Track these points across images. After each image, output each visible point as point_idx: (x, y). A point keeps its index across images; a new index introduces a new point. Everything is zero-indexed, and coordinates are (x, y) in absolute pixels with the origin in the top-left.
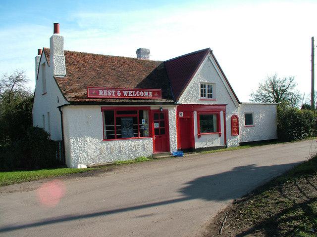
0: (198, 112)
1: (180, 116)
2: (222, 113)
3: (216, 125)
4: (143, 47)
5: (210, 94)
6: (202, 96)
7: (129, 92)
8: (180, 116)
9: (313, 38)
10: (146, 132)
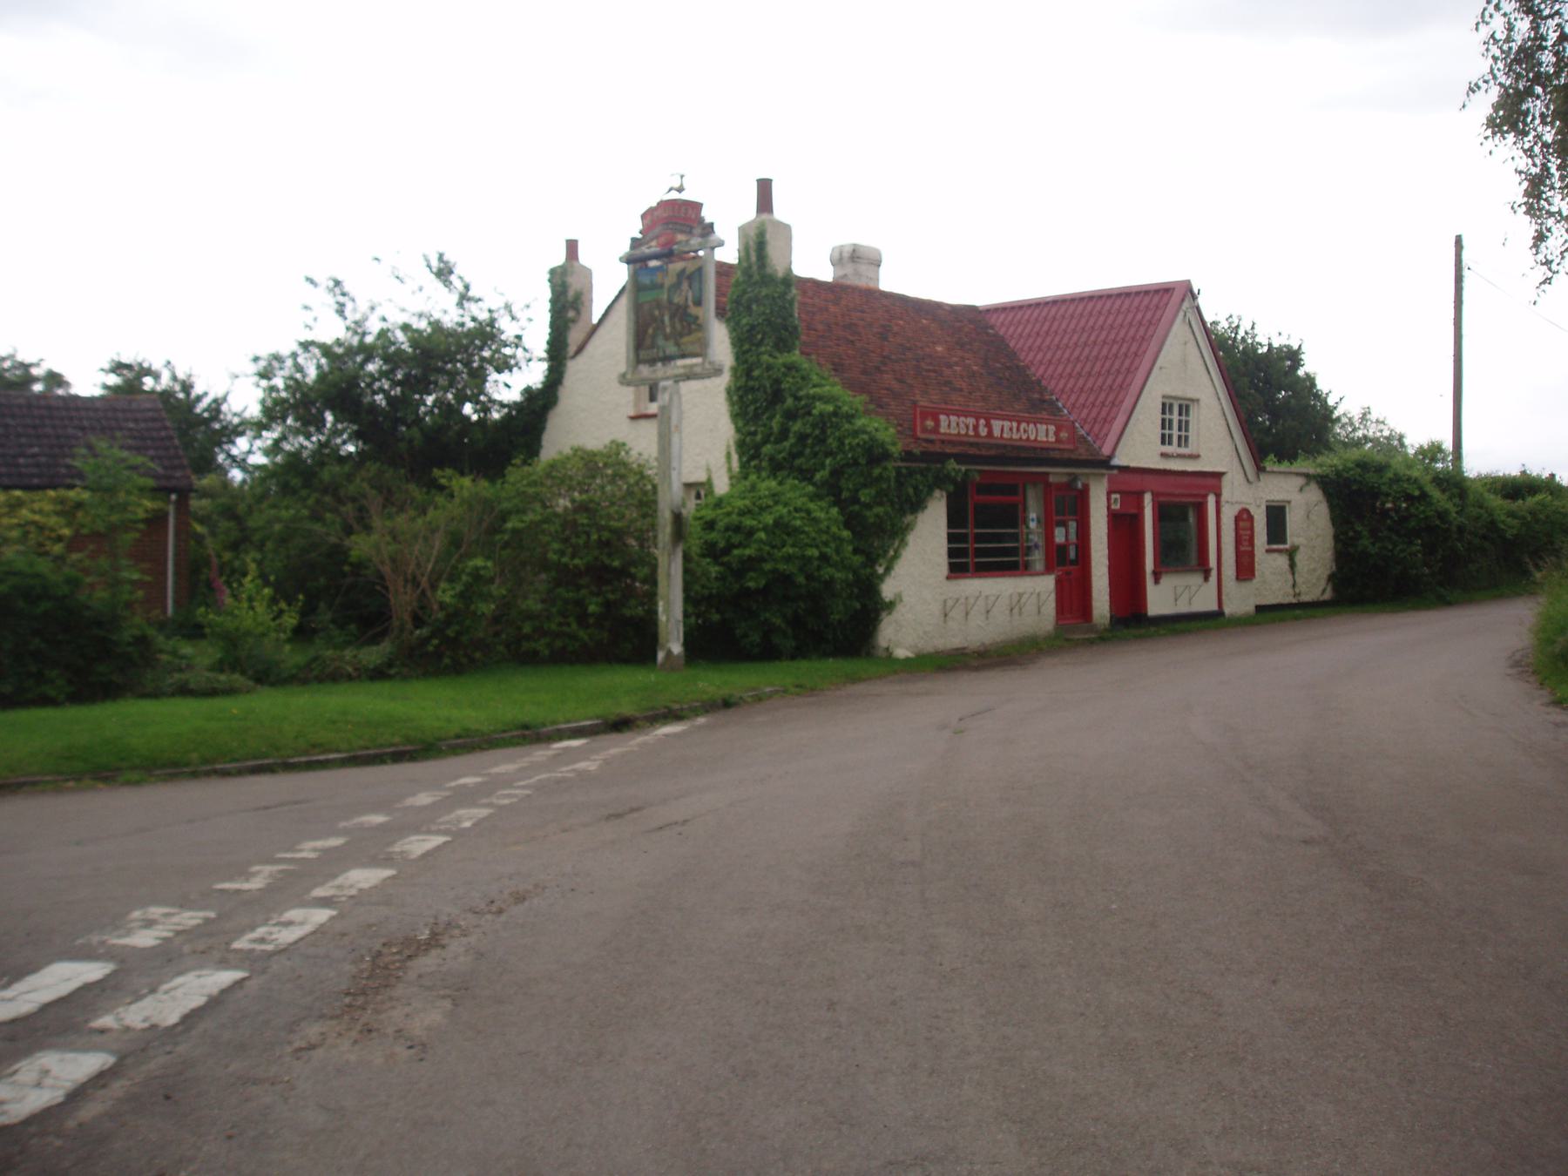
0: (1155, 495)
1: (1113, 507)
2: (1211, 500)
3: (1093, 521)
4: (865, 239)
5: (1183, 433)
6: (1165, 440)
7: (1045, 439)
8: (1113, 507)
9: (1459, 242)
10: (1038, 559)
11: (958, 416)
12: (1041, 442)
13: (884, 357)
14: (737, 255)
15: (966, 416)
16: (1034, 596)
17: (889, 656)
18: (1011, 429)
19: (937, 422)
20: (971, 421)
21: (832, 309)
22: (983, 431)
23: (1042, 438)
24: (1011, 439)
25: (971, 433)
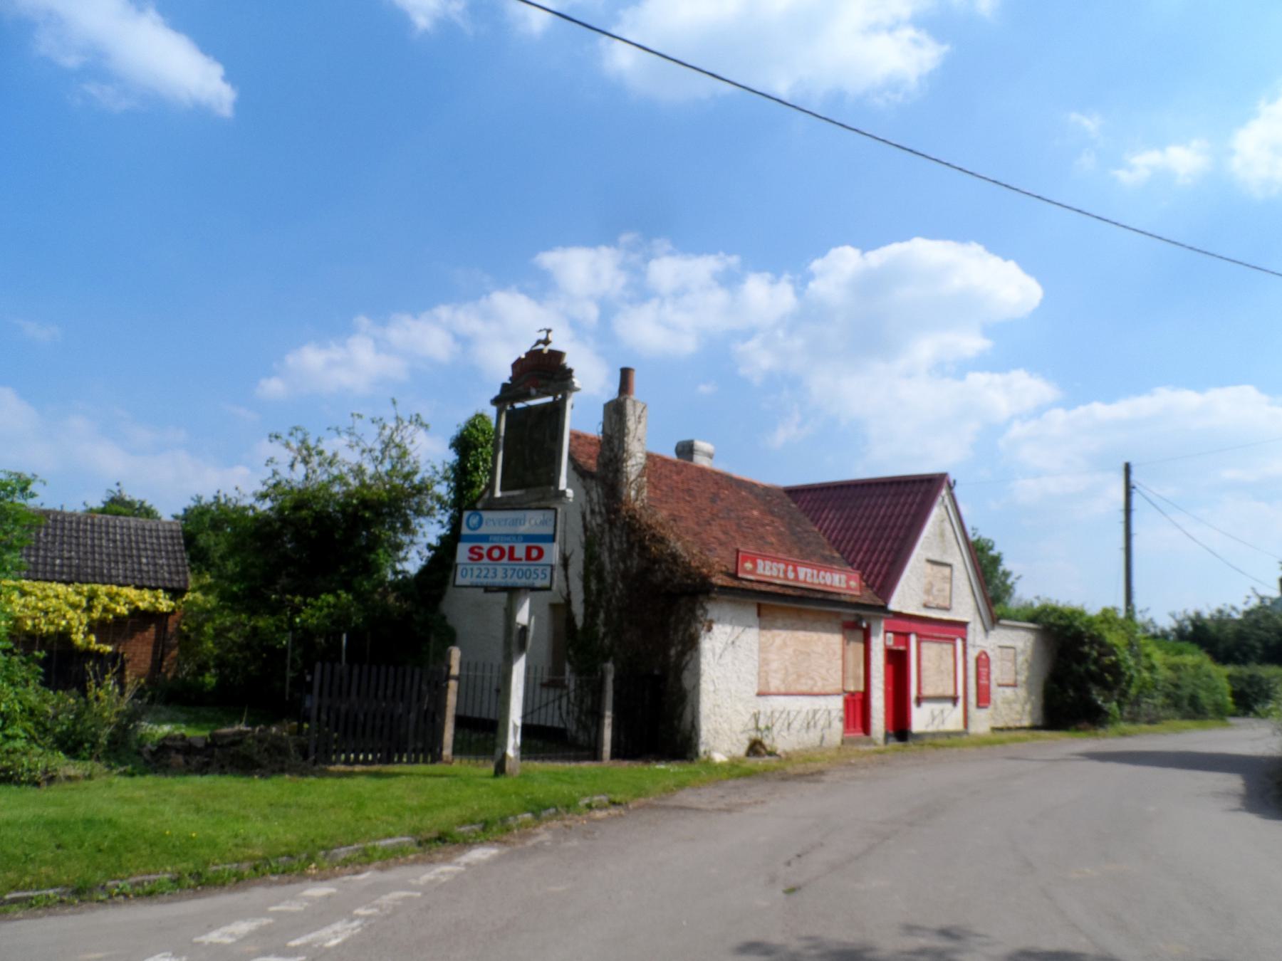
11: (772, 562)
12: (835, 587)
13: (713, 514)
14: (600, 428)
15: (778, 562)
16: (826, 713)
17: (709, 762)
18: (813, 576)
19: (755, 565)
20: (782, 566)
21: (675, 477)
22: (791, 575)
23: (836, 583)
24: (812, 583)
25: (781, 575)
